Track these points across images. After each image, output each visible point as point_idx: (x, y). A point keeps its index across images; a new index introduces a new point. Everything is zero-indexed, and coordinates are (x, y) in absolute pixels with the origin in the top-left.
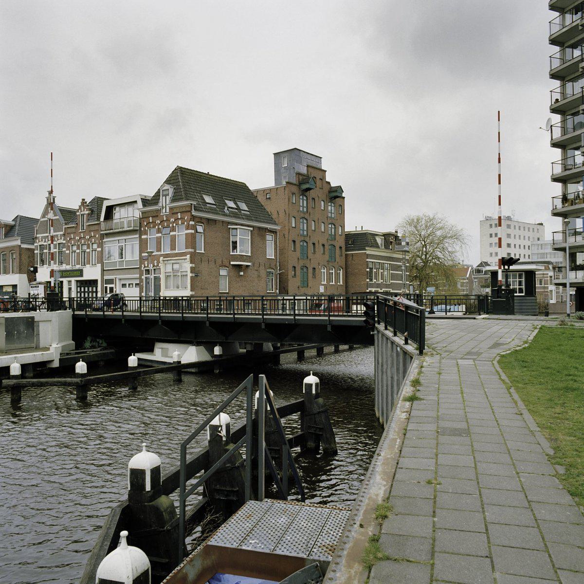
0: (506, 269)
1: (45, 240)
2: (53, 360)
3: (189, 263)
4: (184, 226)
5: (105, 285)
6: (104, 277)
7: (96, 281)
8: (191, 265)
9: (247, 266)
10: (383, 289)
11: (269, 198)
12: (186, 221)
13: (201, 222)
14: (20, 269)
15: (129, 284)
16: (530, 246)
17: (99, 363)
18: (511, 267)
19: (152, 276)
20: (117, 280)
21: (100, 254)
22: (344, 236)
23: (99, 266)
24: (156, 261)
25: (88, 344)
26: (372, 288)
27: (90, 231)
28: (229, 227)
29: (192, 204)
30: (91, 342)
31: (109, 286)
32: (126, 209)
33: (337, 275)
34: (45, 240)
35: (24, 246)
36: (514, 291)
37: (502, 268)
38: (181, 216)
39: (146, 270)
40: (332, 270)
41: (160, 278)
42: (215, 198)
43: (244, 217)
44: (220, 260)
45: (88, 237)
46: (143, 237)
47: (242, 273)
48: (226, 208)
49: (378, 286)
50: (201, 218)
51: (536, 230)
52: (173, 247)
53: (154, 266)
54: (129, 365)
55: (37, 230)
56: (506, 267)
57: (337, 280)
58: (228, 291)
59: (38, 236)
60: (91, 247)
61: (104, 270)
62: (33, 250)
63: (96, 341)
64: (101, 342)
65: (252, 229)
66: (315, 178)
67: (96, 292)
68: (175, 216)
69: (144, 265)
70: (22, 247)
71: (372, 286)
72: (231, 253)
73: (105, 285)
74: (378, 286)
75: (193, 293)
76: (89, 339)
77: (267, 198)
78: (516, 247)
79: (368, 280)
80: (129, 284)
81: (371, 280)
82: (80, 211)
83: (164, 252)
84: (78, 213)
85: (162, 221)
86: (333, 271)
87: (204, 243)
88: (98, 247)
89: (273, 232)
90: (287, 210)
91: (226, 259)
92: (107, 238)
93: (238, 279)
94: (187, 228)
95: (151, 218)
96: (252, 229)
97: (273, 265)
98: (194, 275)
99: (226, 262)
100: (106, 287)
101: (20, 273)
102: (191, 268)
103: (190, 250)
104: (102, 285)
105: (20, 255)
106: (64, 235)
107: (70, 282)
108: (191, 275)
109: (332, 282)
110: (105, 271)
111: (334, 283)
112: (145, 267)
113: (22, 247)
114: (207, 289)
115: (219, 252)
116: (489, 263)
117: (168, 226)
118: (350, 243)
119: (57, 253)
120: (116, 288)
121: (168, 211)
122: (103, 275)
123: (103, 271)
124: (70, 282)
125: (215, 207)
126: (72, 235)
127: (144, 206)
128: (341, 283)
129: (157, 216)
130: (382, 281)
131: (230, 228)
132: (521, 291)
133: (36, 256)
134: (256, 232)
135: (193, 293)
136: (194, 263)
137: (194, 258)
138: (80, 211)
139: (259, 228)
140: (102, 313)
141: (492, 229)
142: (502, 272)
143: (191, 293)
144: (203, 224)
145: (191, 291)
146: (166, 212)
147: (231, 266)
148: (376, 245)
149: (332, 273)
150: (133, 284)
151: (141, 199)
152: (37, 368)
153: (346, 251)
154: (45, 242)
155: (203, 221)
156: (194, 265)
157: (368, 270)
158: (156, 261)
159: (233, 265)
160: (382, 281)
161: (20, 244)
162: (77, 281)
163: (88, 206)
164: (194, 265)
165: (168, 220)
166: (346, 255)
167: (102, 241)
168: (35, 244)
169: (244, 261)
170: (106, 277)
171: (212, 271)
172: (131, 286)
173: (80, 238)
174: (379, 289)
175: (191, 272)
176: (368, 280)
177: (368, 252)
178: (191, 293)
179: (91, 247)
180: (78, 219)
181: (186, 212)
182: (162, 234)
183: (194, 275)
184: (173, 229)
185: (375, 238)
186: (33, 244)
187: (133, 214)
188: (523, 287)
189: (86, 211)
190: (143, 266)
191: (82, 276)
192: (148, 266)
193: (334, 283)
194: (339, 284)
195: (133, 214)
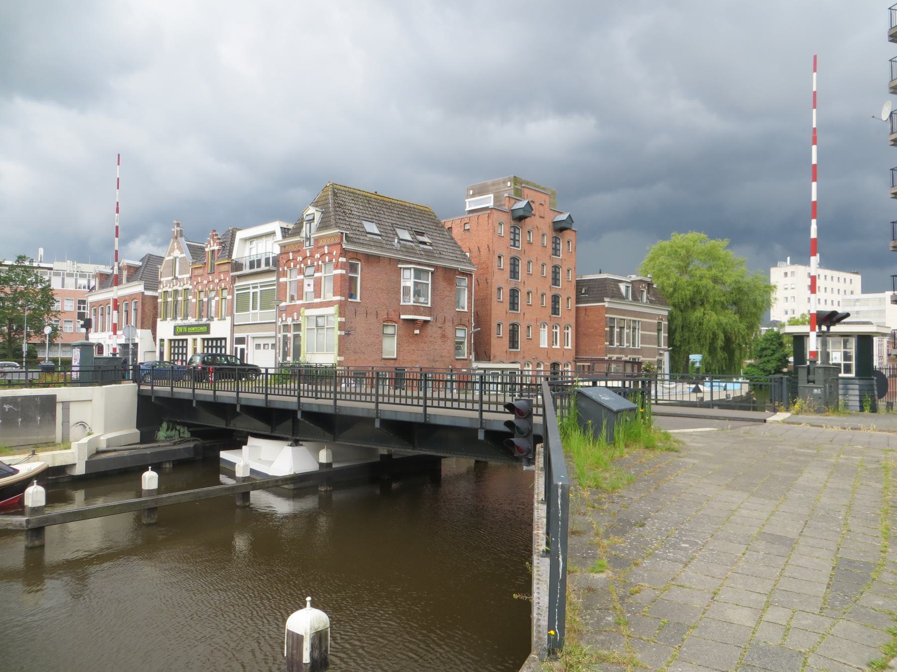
0: (824, 332)
1: (180, 284)
2: (75, 465)
3: (337, 315)
4: (332, 266)
5: (235, 346)
6: (234, 335)
7: (225, 339)
8: (339, 319)
9: (426, 322)
10: (629, 356)
11: (468, 229)
12: (334, 257)
13: (356, 259)
14: (142, 323)
15: (264, 345)
16: (841, 302)
17: (164, 466)
18: (833, 329)
19: (290, 335)
20: (249, 338)
21: (230, 302)
22: (574, 283)
23: (229, 319)
24: (295, 314)
25: (162, 434)
26: (613, 354)
27: (220, 273)
28: (399, 266)
29: (342, 233)
30: (167, 430)
31: (240, 347)
32: (264, 242)
33: (565, 337)
34: (180, 284)
35: (149, 293)
36: (837, 368)
37: (817, 330)
38: (328, 250)
39: (294, 324)
40: (556, 328)
41: (300, 337)
42: (379, 226)
43: (422, 253)
44: (385, 312)
45: (205, 282)
46: (282, 280)
47: (417, 332)
48: (396, 241)
49: (622, 351)
50: (356, 253)
51: (848, 281)
52: (317, 293)
53: (293, 320)
54: (143, 488)
55: (161, 273)
56: (824, 328)
57: (564, 341)
58: (395, 357)
59: (162, 279)
60: (220, 294)
61: (234, 325)
62: (156, 298)
63: (176, 429)
64: (182, 431)
65: (433, 270)
66: (533, 202)
67: (186, 354)
68: (322, 250)
69: (282, 319)
70: (145, 294)
71: (613, 351)
72: (402, 303)
73: (235, 346)
74: (622, 351)
75: (342, 359)
76: (165, 425)
77: (465, 230)
78: (840, 281)
79: (607, 343)
80: (264, 345)
81: (611, 343)
82: (209, 246)
83: (306, 301)
84: (207, 250)
85: (305, 258)
86: (558, 330)
87: (361, 288)
88: (229, 294)
89: (468, 275)
90: (491, 245)
91: (394, 311)
92: (239, 282)
93: (411, 340)
94: (336, 268)
95: (291, 254)
96: (433, 270)
97: (465, 321)
98: (343, 333)
99: (393, 316)
100: (236, 348)
101: (142, 328)
102: (340, 323)
103: (338, 298)
104: (232, 346)
105: (143, 305)
106: (191, 278)
107: (195, 340)
108: (339, 333)
109: (568, 345)
110: (235, 327)
111: (558, 346)
112: (282, 321)
113: (145, 294)
114: (364, 353)
115: (382, 301)
116: (728, 250)
117: (312, 265)
118: (583, 292)
119: (162, 303)
120: (247, 349)
121: (312, 243)
122: (232, 332)
123: (233, 326)
124: (195, 340)
125: (380, 238)
126: (199, 278)
127: (284, 237)
128: (570, 347)
129: (299, 251)
130: (628, 345)
131: (401, 268)
132: (848, 369)
133: (159, 306)
134: (440, 273)
135: (342, 359)
136: (344, 317)
137: (343, 309)
138: (209, 246)
139: (446, 269)
140: (150, 388)
141: (786, 278)
142: (818, 336)
143: (339, 359)
144: (360, 261)
145: (339, 355)
146: (310, 245)
147: (401, 322)
148: (617, 295)
149: (556, 333)
150: (268, 344)
151: (281, 228)
152: (48, 476)
153: (577, 302)
154: (170, 287)
155: (360, 257)
156: (343, 320)
157: (607, 329)
158: (295, 314)
159: (405, 320)
160: (628, 345)
161: (143, 290)
162: (204, 340)
163: (219, 239)
164: (343, 320)
165: (312, 256)
166: (577, 309)
167: (233, 286)
168: (159, 291)
169: (421, 315)
170: (237, 335)
171: (371, 327)
172: (266, 346)
173: (219, 281)
174: (624, 356)
175: (340, 329)
176: (607, 343)
177: (607, 305)
178: (339, 359)
179: (220, 294)
180: (207, 257)
181: (335, 244)
182: (305, 276)
183: (343, 333)
184: (318, 269)
185: (618, 285)
186: (157, 290)
187: (272, 249)
188: (853, 362)
189: (217, 245)
190: (280, 319)
191: (208, 332)
192: (286, 320)
193: (558, 346)
194: (554, 347)
195: (272, 249)
